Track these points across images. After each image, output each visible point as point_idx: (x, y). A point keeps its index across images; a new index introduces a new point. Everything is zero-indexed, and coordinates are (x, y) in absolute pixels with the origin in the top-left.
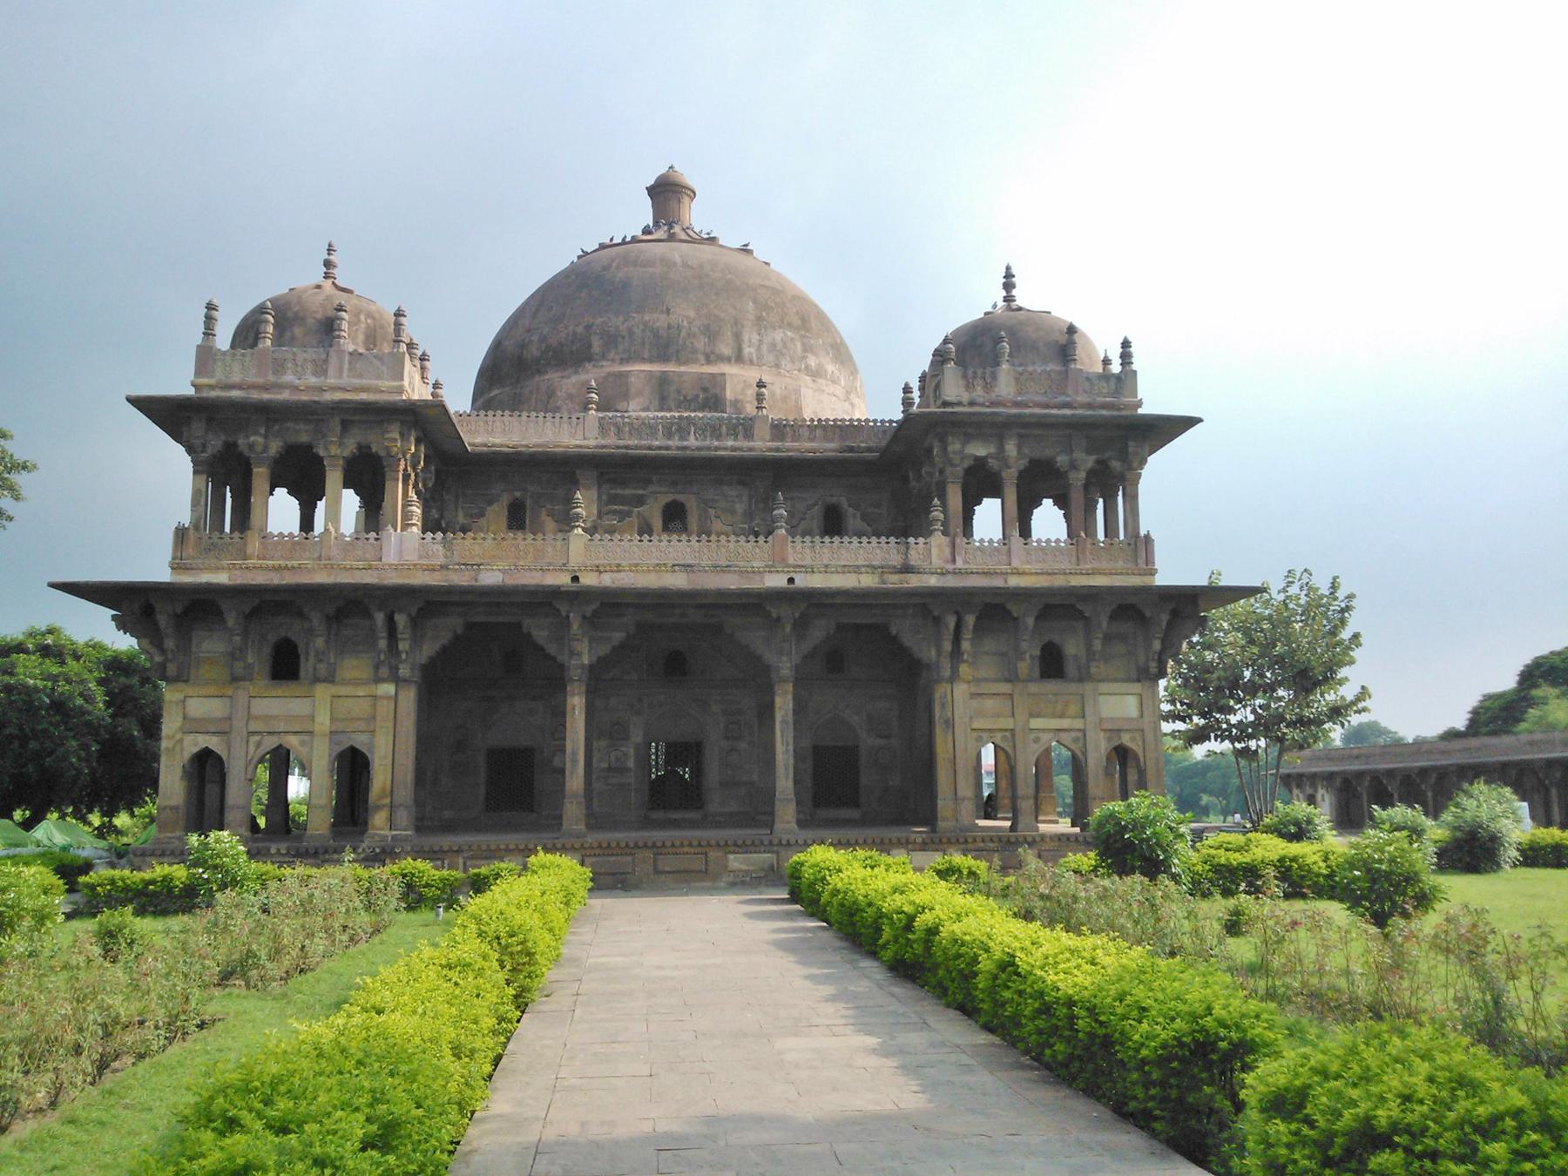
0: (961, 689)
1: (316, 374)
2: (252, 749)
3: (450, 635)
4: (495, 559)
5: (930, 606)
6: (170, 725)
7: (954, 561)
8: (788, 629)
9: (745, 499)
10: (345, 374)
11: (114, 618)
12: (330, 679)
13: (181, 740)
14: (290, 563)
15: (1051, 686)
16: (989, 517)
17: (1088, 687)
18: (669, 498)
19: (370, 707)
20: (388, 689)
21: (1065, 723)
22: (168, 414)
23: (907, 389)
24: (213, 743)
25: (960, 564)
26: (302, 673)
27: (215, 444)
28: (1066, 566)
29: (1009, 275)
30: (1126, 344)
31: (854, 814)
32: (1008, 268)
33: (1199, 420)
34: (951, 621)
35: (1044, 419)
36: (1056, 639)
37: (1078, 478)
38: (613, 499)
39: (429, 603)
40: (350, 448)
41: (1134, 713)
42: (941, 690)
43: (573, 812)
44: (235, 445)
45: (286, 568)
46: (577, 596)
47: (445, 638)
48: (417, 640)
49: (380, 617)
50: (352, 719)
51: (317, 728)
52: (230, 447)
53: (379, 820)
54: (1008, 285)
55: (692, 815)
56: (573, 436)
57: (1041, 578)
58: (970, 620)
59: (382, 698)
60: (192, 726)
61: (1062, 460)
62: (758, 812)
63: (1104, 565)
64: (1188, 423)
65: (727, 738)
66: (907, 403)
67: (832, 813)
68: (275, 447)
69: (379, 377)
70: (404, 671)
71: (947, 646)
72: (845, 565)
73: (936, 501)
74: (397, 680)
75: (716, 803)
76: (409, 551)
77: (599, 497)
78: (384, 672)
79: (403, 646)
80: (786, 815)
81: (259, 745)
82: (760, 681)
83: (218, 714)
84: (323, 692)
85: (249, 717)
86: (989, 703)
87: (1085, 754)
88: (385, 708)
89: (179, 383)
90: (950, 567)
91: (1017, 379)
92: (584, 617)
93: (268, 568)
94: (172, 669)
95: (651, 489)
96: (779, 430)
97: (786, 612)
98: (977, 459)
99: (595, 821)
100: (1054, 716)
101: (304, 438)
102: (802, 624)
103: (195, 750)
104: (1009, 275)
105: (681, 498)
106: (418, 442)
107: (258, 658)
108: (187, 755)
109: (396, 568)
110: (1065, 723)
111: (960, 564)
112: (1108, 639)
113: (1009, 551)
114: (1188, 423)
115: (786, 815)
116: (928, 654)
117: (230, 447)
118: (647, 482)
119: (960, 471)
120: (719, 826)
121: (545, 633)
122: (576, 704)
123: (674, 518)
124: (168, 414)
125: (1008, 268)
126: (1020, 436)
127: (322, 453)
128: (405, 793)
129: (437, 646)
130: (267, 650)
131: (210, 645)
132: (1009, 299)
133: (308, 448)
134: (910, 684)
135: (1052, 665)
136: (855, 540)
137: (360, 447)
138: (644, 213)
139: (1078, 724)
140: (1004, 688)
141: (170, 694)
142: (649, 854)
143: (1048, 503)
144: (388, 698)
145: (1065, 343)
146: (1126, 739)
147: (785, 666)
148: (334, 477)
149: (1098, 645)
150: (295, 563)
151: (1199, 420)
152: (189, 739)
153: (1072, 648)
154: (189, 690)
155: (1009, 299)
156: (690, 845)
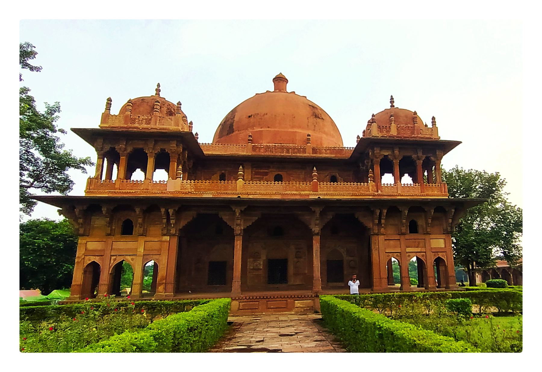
0: (381, 238)
1: (146, 123)
3: (191, 218)
4: (208, 190)
5: (369, 206)
6: (80, 252)
7: (378, 192)
8: (318, 214)
9: (303, 173)
11: (59, 211)
12: (143, 234)
14: (131, 191)
15: (413, 236)
17: (427, 237)
18: (277, 173)
20: (167, 238)
21: (419, 250)
24: (97, 260)
25: (380, 192)
27: (107, 148)
28: (417, 193)
29: (392, 98)
30: (433, 118)
32: (392, 96)
33: (460, 142)
34: (378, 212)
35: (406, 145)
37: (420, 163)
38: (256, 174)
39: (181, 205)
40: (158, 149)
41: (443, 246)
42: (374, 239)
43: (236, 284)
44: (115, 148)
46: (239, 202)
47: (190, 219)
48: (178, 221)
49: (163, 210)
50: (152, 250)
51: (138, 253)
52: (113, 149)
53: (161, 288)
54: (392, 101)
55: (284, 285)
56: (243, 151)
57: (377, 259)
58: (385, 211)
60: (88, 252)
61: (414, 156)
62: (307, 283)
63: (430, 193)
64: (457, 143)
65: (296, 257)
67: (335, 284)
68: (129, 149)
69: (170, 125)
70: (173, 231)
71: (377, 221)
74: (171, 235)
75: (293, 280)
77: (252, 172)
78: (165, 232)
79: (172, 222)
80: (318, 285)
81: (115, 260)
82: (308, 236)
83: (99, 248)
84: (142, 240)
87: (426, 261)
90: (376, 193)
91: (397, 129)
92: (241, 211)
93: (123, 193)
94: (81, 231)
95: (270, 170)
96: (314, 150)
97: (318, 210)
98: (385, 156)
99: (245, 287)
100: (415, 247)
102: (322, 213)
104: (392, 98)
106: (184, 149)
107: (117, 227)
108: (85, 265)
110: (419, 250)
111: (380, 192)
112: (433, 219)
113: (397, 187)
114: (457, 143)
115: (318, 285)
116: (370, 225)
117: (113, 149)
118: (269, 167)
119: (379, 160)
120: (292, 290)
121: (227, 217)
122: (238, 244)
123: (278, 178)
125: (392, 96)
126: (400, 148)
128: (172, 278)
129: (186, 222)
130: (121, 224)
131: (99, 222)
132: (392, 106)
133: (142, 149)
134: (363, 239)
135: (413, 229)
137: (162, 150)
138: (271, 88)
140: (398, 237)
141: (81, 241)
142: (265, 301)
143: (406, 175)
144: (167, 242)
145: (414, 117)
146: (440, 255)
147: (316, 229)
149: (430, 221)
150: (134, 191)
151: (460, 142)
152: (87, 258)
153: (421, 222)
154: (88, 240)
155: (392, 106)
156: (281, 297)
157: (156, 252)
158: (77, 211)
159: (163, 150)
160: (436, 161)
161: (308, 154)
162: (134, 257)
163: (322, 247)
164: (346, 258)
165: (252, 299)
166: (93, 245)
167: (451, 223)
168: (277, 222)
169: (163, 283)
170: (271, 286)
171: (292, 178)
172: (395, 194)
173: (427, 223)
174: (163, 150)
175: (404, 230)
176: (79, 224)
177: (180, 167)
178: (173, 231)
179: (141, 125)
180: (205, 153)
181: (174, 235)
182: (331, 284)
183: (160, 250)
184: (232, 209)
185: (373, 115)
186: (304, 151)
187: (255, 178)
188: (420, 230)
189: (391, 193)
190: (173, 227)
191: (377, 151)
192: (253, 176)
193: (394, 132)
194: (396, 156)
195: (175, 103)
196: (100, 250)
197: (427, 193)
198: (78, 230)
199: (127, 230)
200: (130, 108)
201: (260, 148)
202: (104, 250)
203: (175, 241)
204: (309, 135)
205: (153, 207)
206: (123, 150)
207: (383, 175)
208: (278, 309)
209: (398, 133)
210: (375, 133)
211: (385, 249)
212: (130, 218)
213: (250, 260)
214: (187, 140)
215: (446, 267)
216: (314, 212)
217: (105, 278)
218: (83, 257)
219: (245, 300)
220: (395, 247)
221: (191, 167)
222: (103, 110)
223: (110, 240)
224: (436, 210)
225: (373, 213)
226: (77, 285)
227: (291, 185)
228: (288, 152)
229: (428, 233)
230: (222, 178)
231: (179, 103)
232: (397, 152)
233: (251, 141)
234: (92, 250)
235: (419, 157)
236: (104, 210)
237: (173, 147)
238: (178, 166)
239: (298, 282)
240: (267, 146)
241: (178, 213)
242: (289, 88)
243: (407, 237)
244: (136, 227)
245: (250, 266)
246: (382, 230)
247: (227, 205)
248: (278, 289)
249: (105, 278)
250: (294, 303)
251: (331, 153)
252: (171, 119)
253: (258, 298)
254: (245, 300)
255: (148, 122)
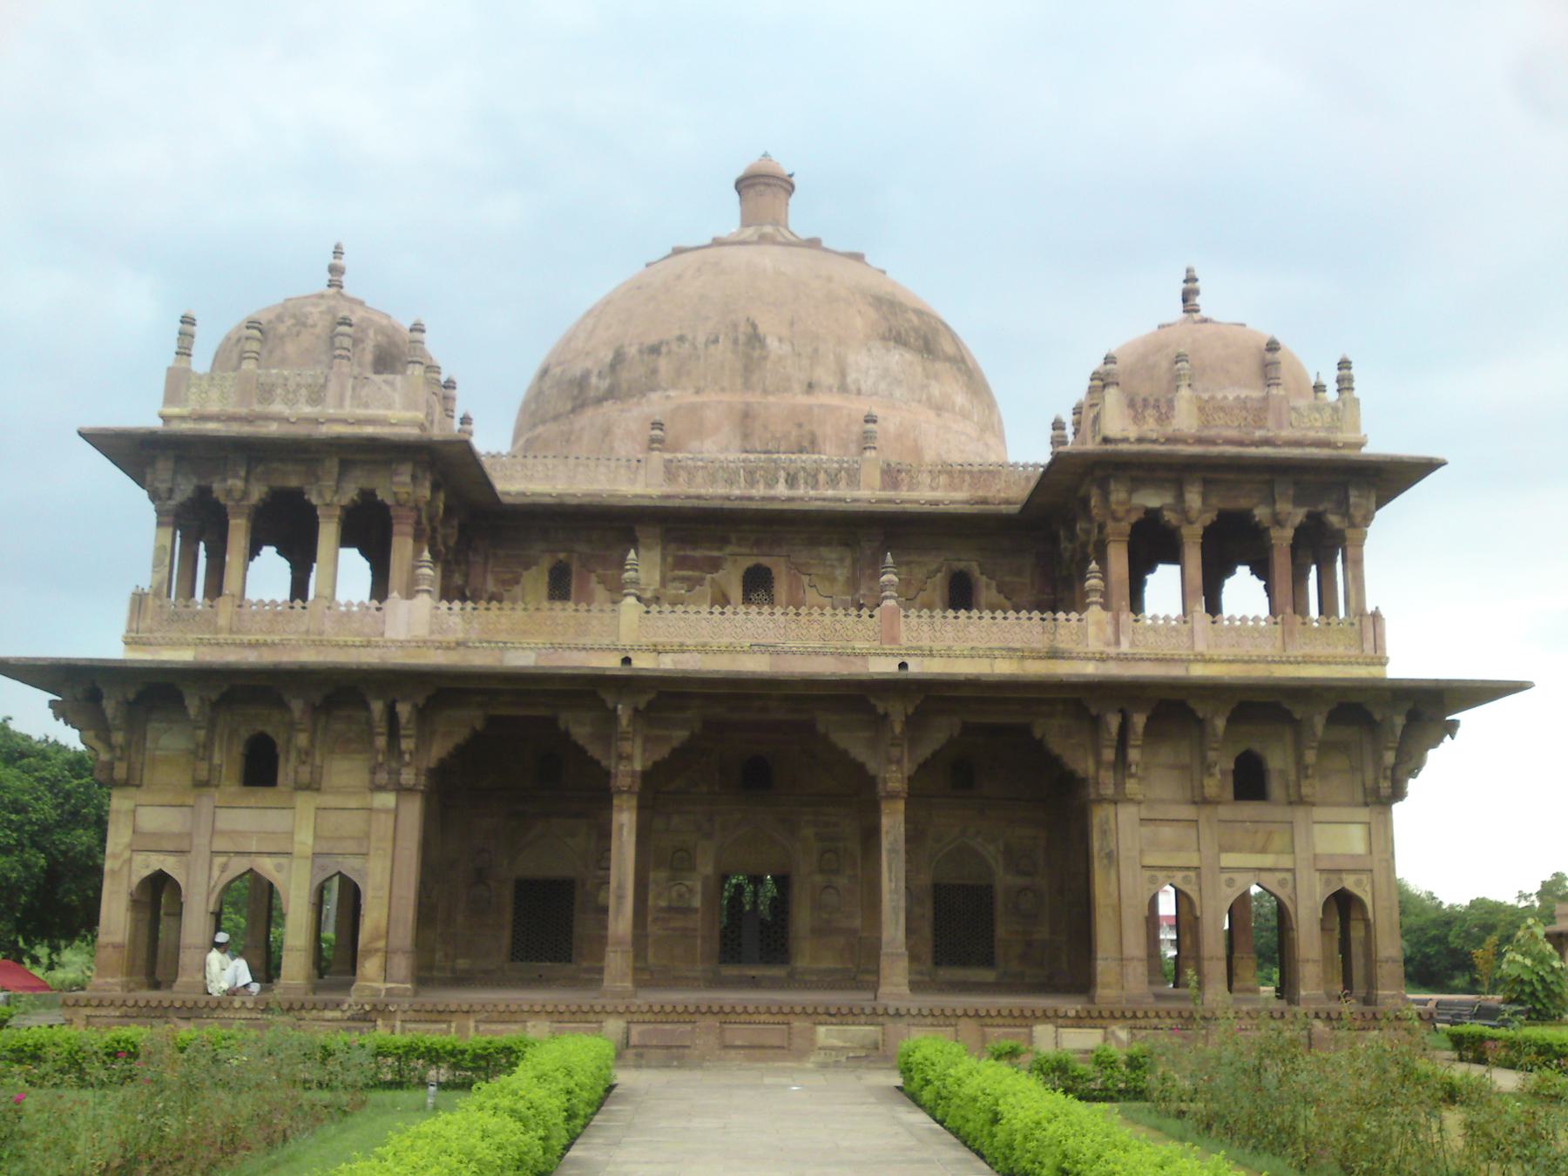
0: (1127, 815)
2: (216, 873)
4: (524, 635)
6: (118, 839)
7: (1118, 643)
8: (898, 729)
9: (848, 562)
10: (348, 402)
11: (52, 704)
12: (313, 786)
13: (130, 860)
14: (269, 639)
15: (1249, 809)
16: (1165, 588)
17: (1299, 813)
18: (750, 562)
19: (351, 832)
20: (388, 800)
22: (132, 452)
23: (1058, 425)
24: (169, 865)
25: (1125, 647)
26: (280, 778)
27: (186, 489)
29: (1190, 279)
30: (1344, 365)
31: (989, 975)
34: (1114, 722)
36: (1256, 747)
37: (1282, 538)
38: (681, 563)
39: (439, 691)
40: (350, 493)
42: (1099, 815)
43: (617, 962)
45: (265, 644)
46: (627, 684)
47: (460, 735)
48: (423, 739)
49: (377, 707)
51: (297, 849)
52: (204, 493)
54: (335, 270)
58: (1139, 720)
59: (379, 811)
60: (143, 842)
61: (1261, 513)
63: (1319, 650)
66: (1057, 441)
67: (959, 974)
68: (257, 493)
69: (389, 407)
71: (1109, 754)
72: (984, 645)
73: (1093, 566)
74: (401, 790)
75: (805, 957)
76: (418, 626)
77: (664, 558)
79: (407, 744)
81: (224, 868)
82: (862, 796)
83: (176, 828)
84: (306, 803)
85: (214, 832)
86: (1167, 832)
88: (384, 824)
89: (143, 412)
90: (1112, 651)
93: (242, 645)
94: (120, 771)
95: (729, 549)
96: (891, 476)
97: (898, 713)
101: (293, 482)
102: (915, 724)
103: (146, 873)
105: (765, 561)
106: (435, 487)
107: (227, 759)
108: (136, 880)
109: (402, 645)
110: (1267, 860)
113: (1192, 630)
116: (1084, 765)
117: (204, 493)
118: (725, 541)
119: (1125, 527)
120: (807, 986)
122: (625, 821)
123: (757, 585)
124: (132, 452)
126: (1206, 483)
127: (314, 500)
128: (404, 934)
130: (238, 750)
135: (1250, 782)
136: (987, 614)
138: (726, 216)
139: (1286, 861)
140: (1188, 812)
141: (119, 803)
143: (1243, 571)
144: (387, 811)
146: (1349, 883)
147: (894, 778)
148: (328, 533)
150: (277, 638)
152: (139, 859)
153: (1277, 760)
157: (350, 846)
158: (109, 707)
159: (367, 496)
160: (1349, 533)
161: (867, 493)
162: (283, 860)
163: (914, 837)
164: (1004, 880)
165: (662, 1014)
166: (155, 818)
167: (1394, 768)
168: (757, 755)
169: (377, 950)
170: (730, 971)
171: (805, 579)
172: (1183, 652)
173: (1302, 768)
174: (367, 496)
175: (1212, 786)
176: (111, 747)
177: (426, 555)
178: (407, 777)
179: (291, 412)
180: (501, 486)
181: (410, 790)
182: (946, 973)
183: (367, 835)
184: (603, 701)
185: (1109, 360)
186: (853, 478)
187: (674, 579)
188: (1275, 788)
189: (1167, 651)
190: (408, 764)
191: (1118, 494)
192: (670, 575)
193: (1185, 420)
194: (1196, 509)
195: (407, 324)
196: (179, 835)
197: (1308, 650)
198: (110, 766)
199: (260, 769)
200: (255, 346)
201: (691, 473)
202: (190, 835)
203: (413, 811)
204: (871, 419)
205: (345, 699)
206: (237, 495)
207: (1152, 570)
208: (757, 1051)
209: (1206, 425)
210: (1119, 425)
211: (1142, 852)
212: (269, 730)
213: (657, 876)
214: (449, 465)
215: (1368, 925)
216: (886, 715)
217: (1309, 940)
218: (127, 854)
219: (647, 1017)
220: (1179, 848)
221: (452, 543)
222: (169, 359)
223: (206, 804)
224: (1334, 718)
225: (1096, 722)
226: (115, 946)
227: (803, 619)
228: (791, 481)
229: (1300, 801)
230: (560, 587)
231: (418, 328)
232: (1194, 499)
233: (661, 441)
234: (154, 835)
235: (1284, 518)
236: (193, 705)
237: (401, 488)
238: (417, 553)
239: (828, 963)
240: (715, 468)
241: (423, 715)
242: (801, 217)
243: (1224, 812)
244: (287, 760)
245: (655, 901)
246: (1131, 786)
247: (587, 690)
248: (754, 983)
249: (1309, 940)
250: (814, 1032)
251: (952, 486)
252: (392, 384)
253: (692, 1009)
254: (647, 1017)
255: (316, 397)
